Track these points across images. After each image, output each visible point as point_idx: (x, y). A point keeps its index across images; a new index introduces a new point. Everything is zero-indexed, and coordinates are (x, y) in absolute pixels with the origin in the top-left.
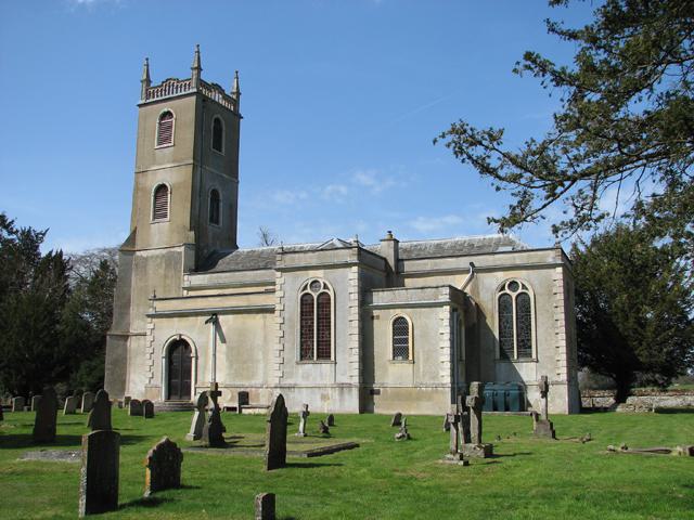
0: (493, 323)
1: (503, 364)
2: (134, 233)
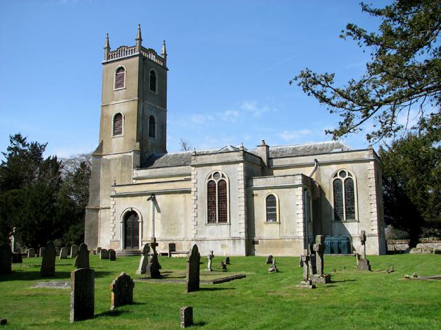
2: (101, 144)
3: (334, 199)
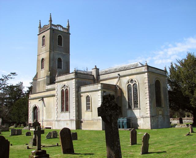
0: (126, 95)
1: (129, 111)
2: (37, 74)
3: (128, 96)
